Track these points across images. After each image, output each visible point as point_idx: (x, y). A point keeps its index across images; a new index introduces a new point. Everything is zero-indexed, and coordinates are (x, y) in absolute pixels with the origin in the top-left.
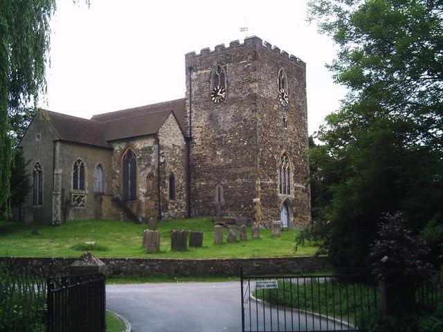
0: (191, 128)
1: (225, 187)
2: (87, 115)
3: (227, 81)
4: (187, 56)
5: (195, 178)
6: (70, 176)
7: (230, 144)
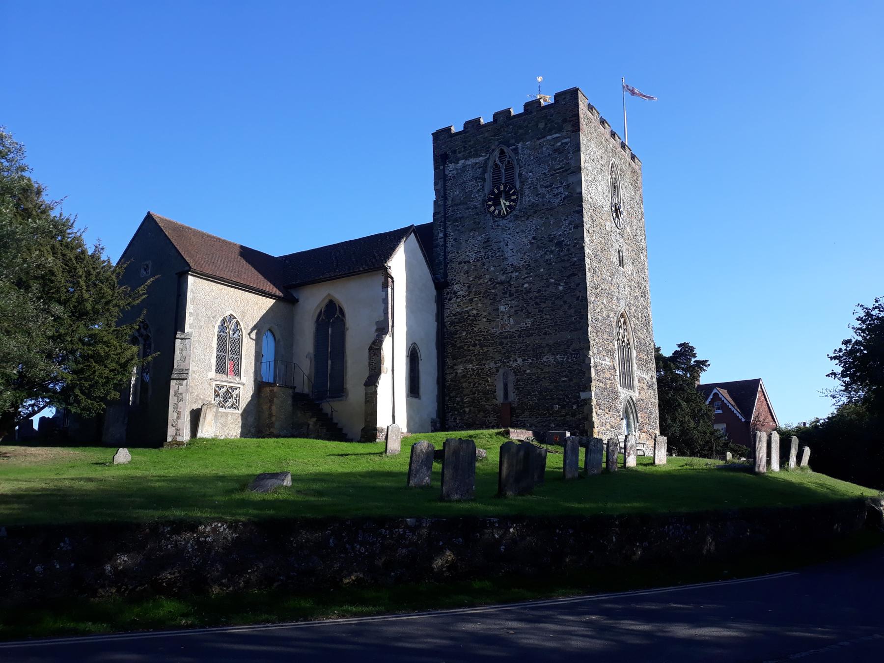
1: (517, 372)
3: (520, 175)
4: (437, 136)
5: (454, 358)
6: (211, 347)
7: (528, 291)
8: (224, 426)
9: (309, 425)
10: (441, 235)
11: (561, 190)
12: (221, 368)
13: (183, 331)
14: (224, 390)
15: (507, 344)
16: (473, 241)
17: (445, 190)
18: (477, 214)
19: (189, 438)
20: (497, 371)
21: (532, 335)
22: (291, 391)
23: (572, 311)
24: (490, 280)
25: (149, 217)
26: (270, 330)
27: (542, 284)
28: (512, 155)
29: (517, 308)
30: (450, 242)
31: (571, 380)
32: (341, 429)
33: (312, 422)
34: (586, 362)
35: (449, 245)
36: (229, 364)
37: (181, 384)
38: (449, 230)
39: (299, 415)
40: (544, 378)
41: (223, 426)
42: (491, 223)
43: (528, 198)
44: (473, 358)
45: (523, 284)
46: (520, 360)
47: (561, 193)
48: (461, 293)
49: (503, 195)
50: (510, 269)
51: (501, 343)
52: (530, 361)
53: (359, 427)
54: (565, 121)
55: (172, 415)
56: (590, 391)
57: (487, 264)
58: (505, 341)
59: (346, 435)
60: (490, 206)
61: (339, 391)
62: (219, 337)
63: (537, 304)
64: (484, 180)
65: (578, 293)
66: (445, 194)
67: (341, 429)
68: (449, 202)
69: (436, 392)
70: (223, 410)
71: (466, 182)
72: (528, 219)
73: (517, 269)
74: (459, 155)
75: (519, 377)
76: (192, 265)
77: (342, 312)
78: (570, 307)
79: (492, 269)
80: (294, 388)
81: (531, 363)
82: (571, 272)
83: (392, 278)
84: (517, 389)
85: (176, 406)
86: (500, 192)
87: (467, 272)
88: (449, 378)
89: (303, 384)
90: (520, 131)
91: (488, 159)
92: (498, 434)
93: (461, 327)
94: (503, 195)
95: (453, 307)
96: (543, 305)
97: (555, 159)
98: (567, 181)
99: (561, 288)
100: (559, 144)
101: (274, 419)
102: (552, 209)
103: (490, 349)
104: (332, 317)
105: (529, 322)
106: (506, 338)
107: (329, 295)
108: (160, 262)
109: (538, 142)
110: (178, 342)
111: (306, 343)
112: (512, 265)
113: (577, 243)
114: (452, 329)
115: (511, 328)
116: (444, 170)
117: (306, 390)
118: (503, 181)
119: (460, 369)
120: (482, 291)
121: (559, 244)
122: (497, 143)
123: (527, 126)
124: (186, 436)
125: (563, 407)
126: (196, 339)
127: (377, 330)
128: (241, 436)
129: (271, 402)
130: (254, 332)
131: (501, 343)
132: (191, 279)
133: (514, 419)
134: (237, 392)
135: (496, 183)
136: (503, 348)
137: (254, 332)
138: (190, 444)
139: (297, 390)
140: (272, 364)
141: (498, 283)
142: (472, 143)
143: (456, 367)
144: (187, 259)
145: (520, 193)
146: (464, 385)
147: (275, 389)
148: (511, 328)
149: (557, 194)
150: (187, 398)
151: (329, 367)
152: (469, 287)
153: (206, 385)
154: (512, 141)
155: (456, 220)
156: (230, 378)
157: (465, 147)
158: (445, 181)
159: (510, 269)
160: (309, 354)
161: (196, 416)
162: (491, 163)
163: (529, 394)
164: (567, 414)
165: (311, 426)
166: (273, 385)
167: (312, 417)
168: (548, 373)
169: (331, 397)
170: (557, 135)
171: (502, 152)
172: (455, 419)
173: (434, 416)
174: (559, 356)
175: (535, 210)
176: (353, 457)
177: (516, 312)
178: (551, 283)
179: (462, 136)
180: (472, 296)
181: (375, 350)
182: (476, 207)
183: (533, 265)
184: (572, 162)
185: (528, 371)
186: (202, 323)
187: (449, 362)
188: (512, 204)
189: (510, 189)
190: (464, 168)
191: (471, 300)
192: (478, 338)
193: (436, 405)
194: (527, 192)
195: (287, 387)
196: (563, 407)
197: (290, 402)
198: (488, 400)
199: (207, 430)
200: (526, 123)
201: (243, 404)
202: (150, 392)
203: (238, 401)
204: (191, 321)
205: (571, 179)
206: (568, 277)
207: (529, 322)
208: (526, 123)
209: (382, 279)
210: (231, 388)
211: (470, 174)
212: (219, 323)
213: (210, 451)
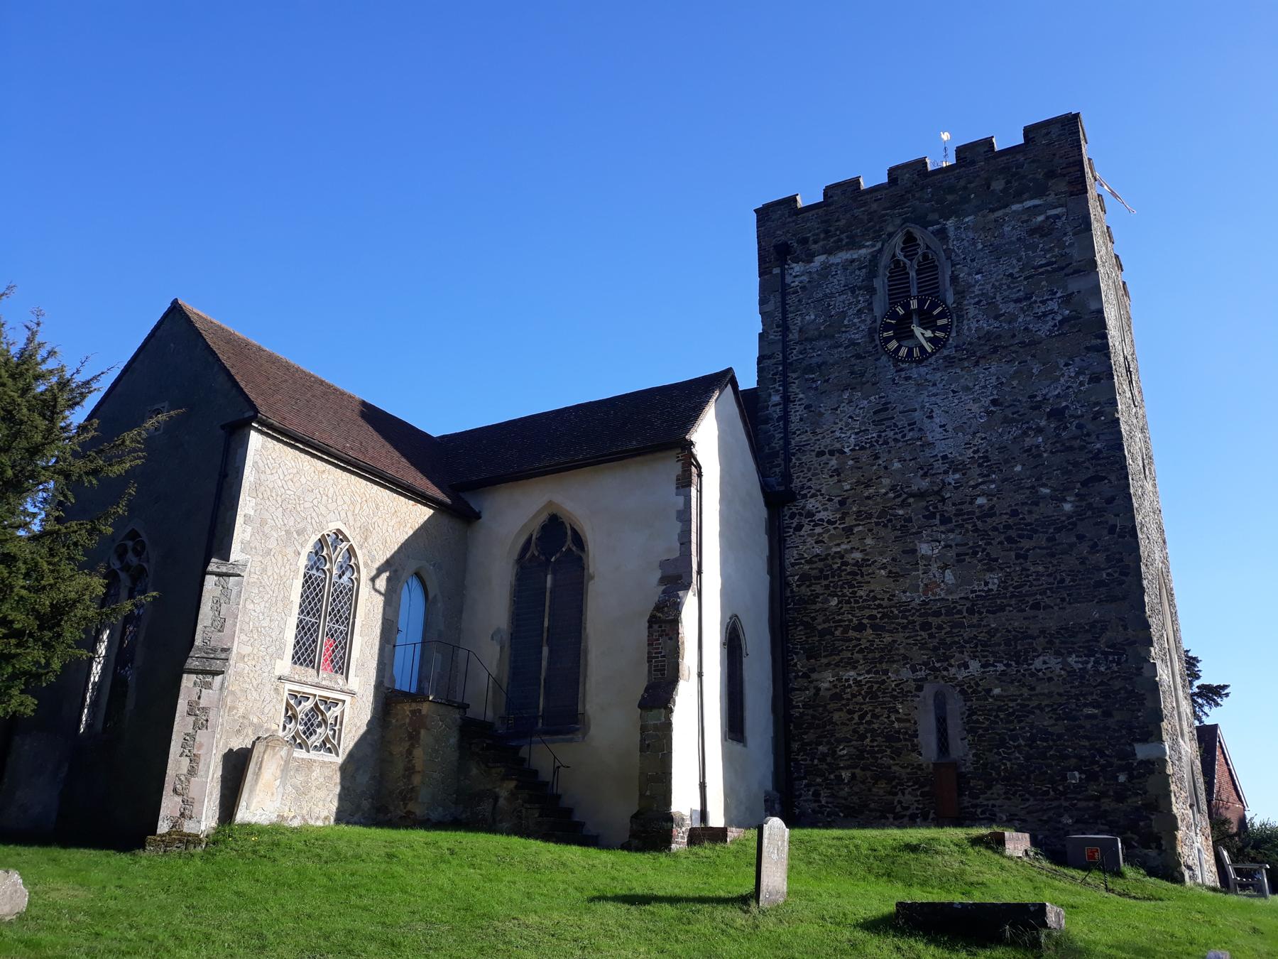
0: (787, 460)
1: (968, 690)
2: (435, 433)
3: (954, 279)
4: (764, 214)
5: (811, 654)
6: (286, 598)
7: (989, 513)
8: (302, 792)
9: (496, 799)
10: (776, 398)
11: (1053, 305)
12: (304, 654)
13: (225, 557)
14: (308, 705)
15: (940, 628)
16: (849, 410)
17: (784, 312)
18: (858, 356)
19: (213, 823)
20: (920, 688)
21: (1002, 608)
22: (456, 715)
23: (1100, 558)
24: (893, 488)
25: (176, 310)
26: (417, 575)
27: (1021, 497)
28: (935, 243)
29: (960, 549)
30: (797, 412)
31: (1108, 714)
32: (569, 811)
33: (505, 789)
34: (1146, 672)
35: (794, 418)
36: (324, 644)
37: (209, 686)
38: (794, 388)
39: (474, 771)
40: (1039, 707)
41: (295, 794)
42: (891, 372)
43: (975, 323)
44: (857, 656)
45: (974, 498)
46: (975, 666)
47: (1052, 311)
48: (823, 515)
49: (915, 319)
50: (939, 466)
51: (926, 626)
52: (1001, 667)
53: (621, 811)
54: (1051, 174)
55: (176, 764)
56: (1161, 740)
57: (884, 457)
58: (934, 621)
59: (582, 825)
60: (888, 340)
61: (567, 719)
62: (308, 579)
63: (1010, 540)
64: (872, 291)
65: (1111, 519)
66: (784, 319)
67: (569, 811)
68: (794, 335)
69: (770, 733)
70: (300, 754)
71: (832, 295)
72: (977, 364)
73: (955, 466)
74: (814, 247)
75: (975, 703)
76: (262, 409)
77: (579, 541)
78: (1094, 547)
79: (897, 465)
80: (464, 707)
81: (1003, 673)
82: (1090, 473)
83: (699, 467)
84: (971, 731)
85: (189, 739)
86: (909, 313)
87: (837, 472)
88: (799, 698)
89: (484, 706)
90: (950, 198)
91: (881, 250)
92: (976, 842)
93: (827, 587)
94: (915, 319)
95: (805, 545)
96: (1026, 544)
97: (1034, 247)
98: (1065, 288)
99: (1067, 507)
100: (1040, 218)
101: (417, 780)
102: (1034, 343)
103: (900, 637)
104: (556, 548)
105: (994, 580)
106: (937, 614)
107: (550, 503)
108: (192, 410)
109: (993, 216)
110: (210, 581)
111: (493, 606)
112: (945, 457)
113: (1100, 413)
114: (804, 590)
115: (949, 592)
116: (783, 275)
117: (490, 716)
118: (914, 291)
119: (826, 680)
120: (876, 511)
121: (1057, 414)
122: (898, 221)
123: (965, 188)
124: (206, 820)
125: (1092, 777)
126: (254, 578)
127: (663, 580)
128: (338, 820)
129: (414, 738)
130: (385, 576)
131: (926, 626)
132: (256, 441)
133: (966, 801)
134: (336, 711)
135: (898, 293)
136: (931, 636)
137: (385, 576)
138: (215, 840)
139: (469, 714)
140: (418, 647)
141: (911, 495)
142: (843, 222)
143: (814, 676)
144: (252, 396)
145: (958, 313)
146: (836, 716)
147: (425, 708)
148: (949, 592)
149: (1045, 315)
150: (221, 720)
151: (544, 663)
152: (842, 503)
153: (268, 690)
154: (931, 217)
155: (809, 369)
156: (325, 677)
157: (827, 232)
158: (784, 295)
159: (939, 466)
160: (498, 631)
161: (237, 768)
162: (885, 260)
163: (1002, 743)
164: (1103, 794)
165: (502, 802)
166: (419, 696)
167: (505, 778)
168: (1050, 695)
169: (546, 733)
170: (1037, 202)
171: (910, 239)
172: (816, 794)
173: (769, 786)
174: (1072, 659)
175: (992, 345)
176: (668, 910)
177: (960, 558)
178: (1044, 497)
179: (820, 211)
180: (850, 521)
181: (664, 623)
182: (853, 343)
183: (995, 456)
184: (1075, 253)
185: (997, 691)
186: (272, 544)
187: (800, 663)
188: (938, 334)
189: (934, 306)
190: (826, 270)
191: (849, 531)
192: (867, 612)
193: (770, 760)
194: (972, 311)
195: (449, 703)
196: (1092, 777)
197: (453, 740)
198: (897, 753)
199: (259, 806)
200: (962, 183)
201: (348, 741)
202: (130, 703)
203: (337, 734)
204: (247, 536)
205: (1074, 285)
206: (1084, 484)
207: (994, 580)
208: (962, 183)
209: (677, 468)
210: (324, 700)
211: (839, 280)
212: (310, 547)
213: (268, 868)
